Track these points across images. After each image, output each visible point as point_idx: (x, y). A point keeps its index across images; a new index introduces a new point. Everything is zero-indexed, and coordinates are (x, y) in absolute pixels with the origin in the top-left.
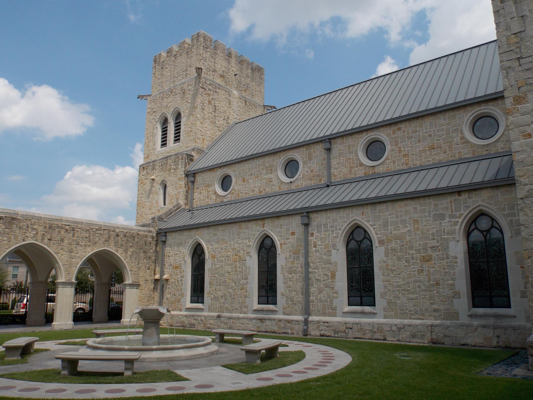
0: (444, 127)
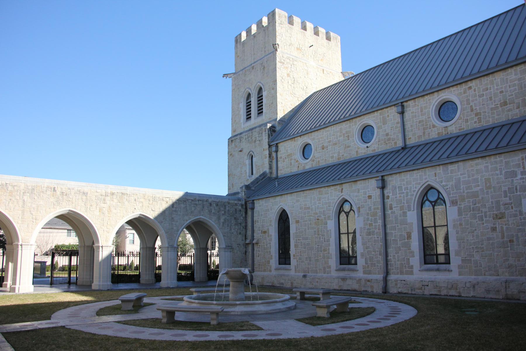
0: (515, 82)
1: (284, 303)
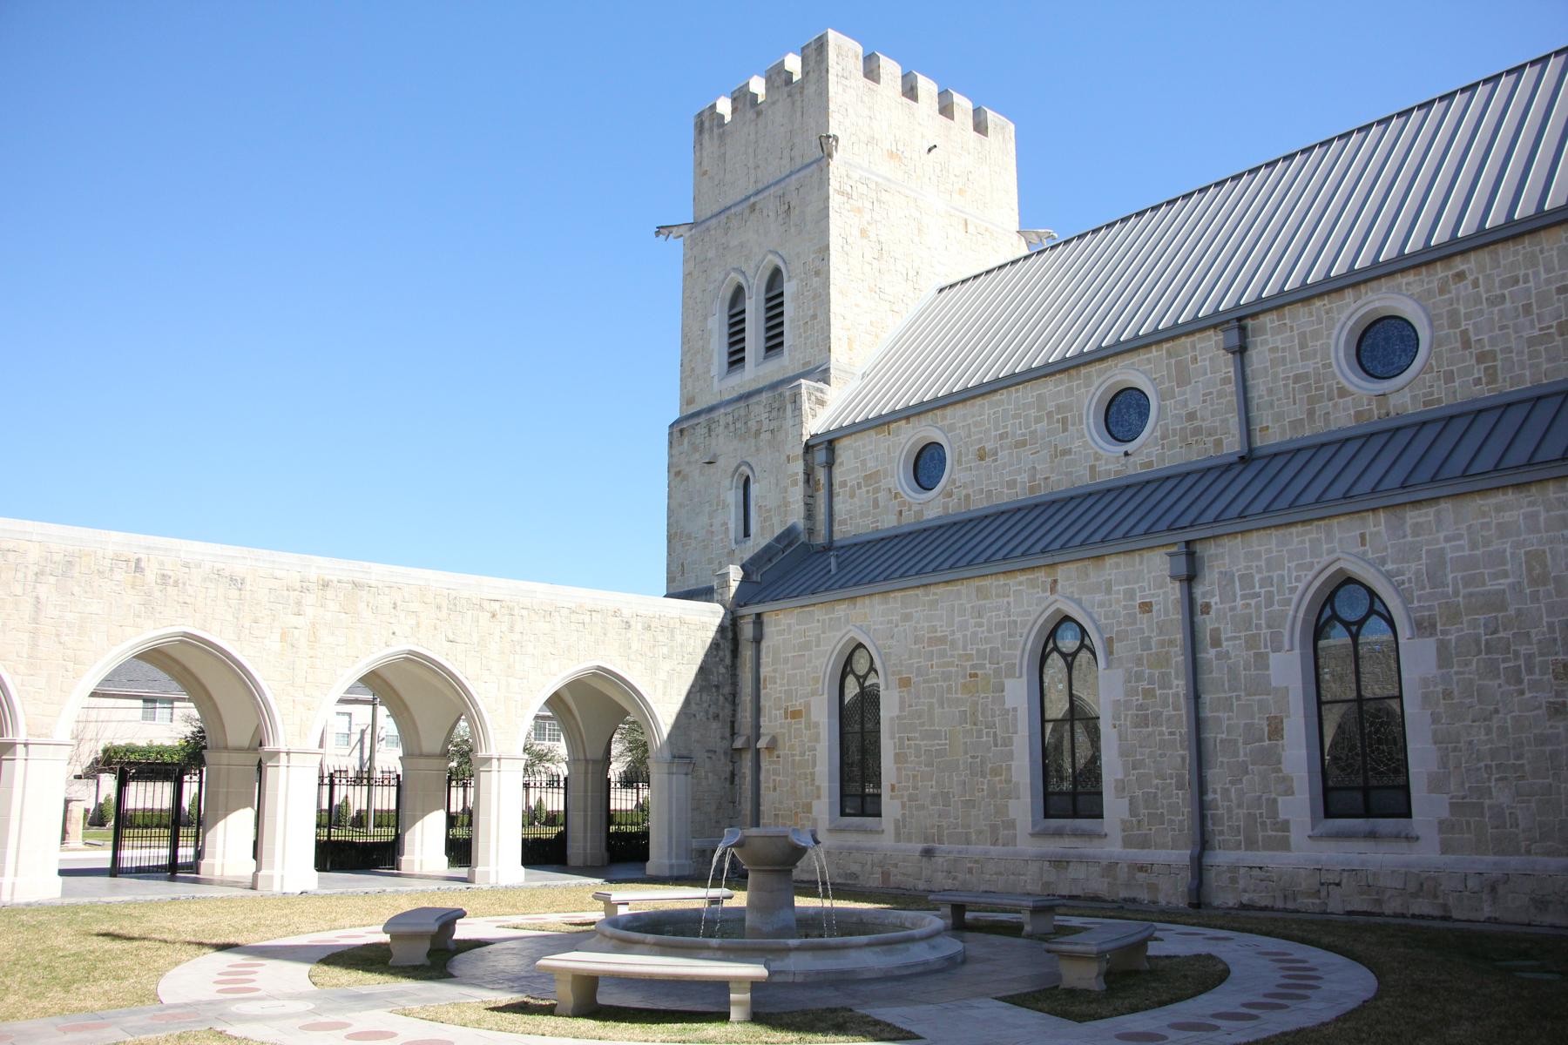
1: (933, 942)
